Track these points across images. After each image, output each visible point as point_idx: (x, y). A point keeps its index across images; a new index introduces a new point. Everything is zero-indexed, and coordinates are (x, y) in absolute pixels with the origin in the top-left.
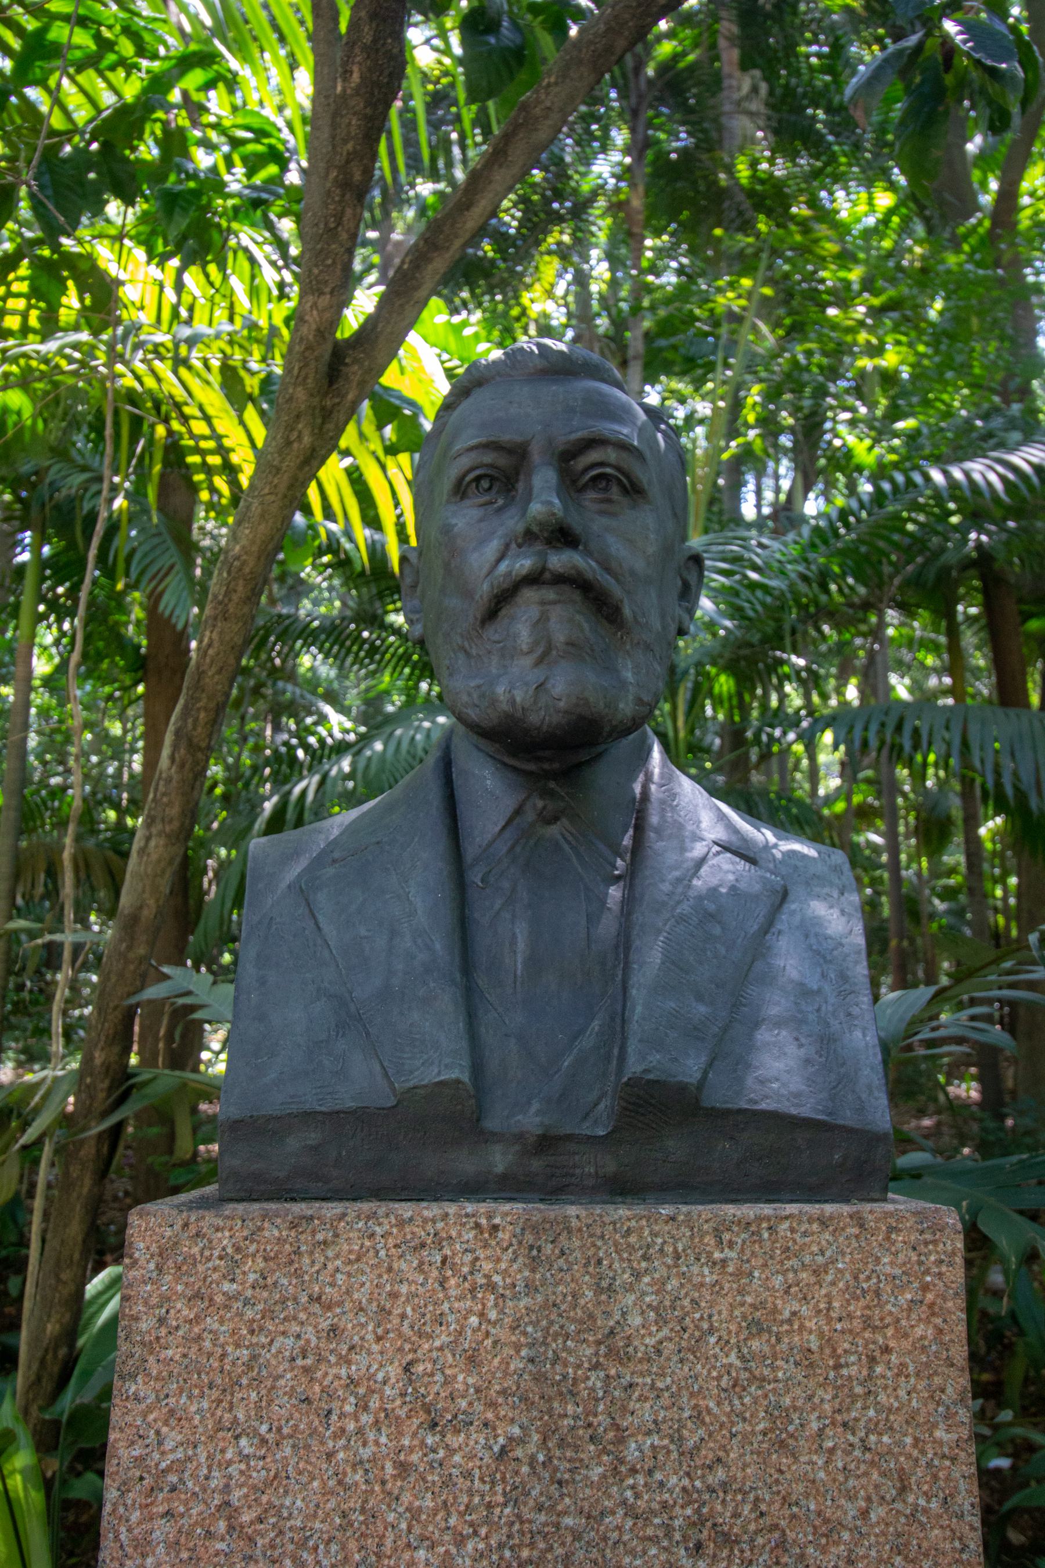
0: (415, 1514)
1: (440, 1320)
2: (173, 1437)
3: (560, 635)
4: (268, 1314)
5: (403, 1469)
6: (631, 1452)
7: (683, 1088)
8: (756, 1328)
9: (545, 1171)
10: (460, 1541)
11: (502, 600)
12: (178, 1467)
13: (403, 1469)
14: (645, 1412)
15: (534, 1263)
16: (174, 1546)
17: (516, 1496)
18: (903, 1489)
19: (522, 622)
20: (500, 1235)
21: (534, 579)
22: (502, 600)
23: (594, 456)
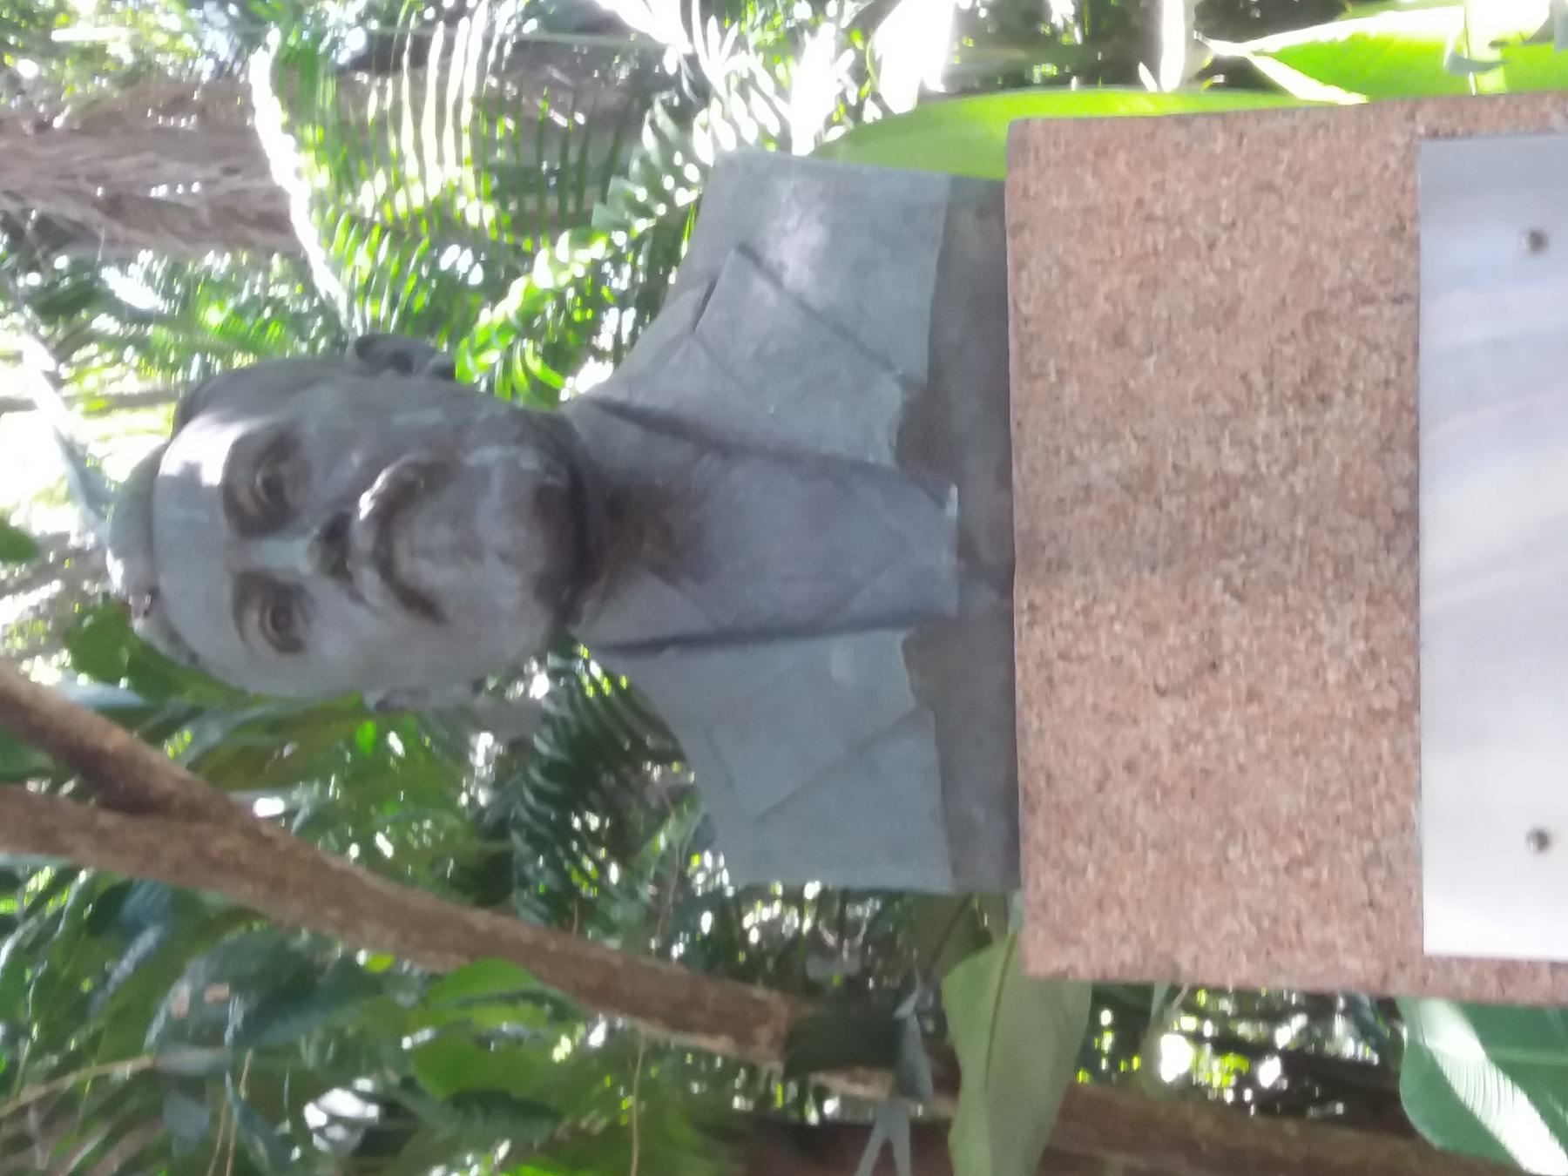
0: (1294, 684)
1: (1117, 661)
3: (442, 535)
4: (1114, 832)
5: (1253, 695)
6: (1236, 467)
8: (1119, 339)
9: (992, 565)
10: (1318, 639)
12: (1255, 918)
13: (1253, 695)
16: (1325, 920)
17: (1277, 584)
18: (1269, 187)
19: (433, 575)
21: (386, 568)
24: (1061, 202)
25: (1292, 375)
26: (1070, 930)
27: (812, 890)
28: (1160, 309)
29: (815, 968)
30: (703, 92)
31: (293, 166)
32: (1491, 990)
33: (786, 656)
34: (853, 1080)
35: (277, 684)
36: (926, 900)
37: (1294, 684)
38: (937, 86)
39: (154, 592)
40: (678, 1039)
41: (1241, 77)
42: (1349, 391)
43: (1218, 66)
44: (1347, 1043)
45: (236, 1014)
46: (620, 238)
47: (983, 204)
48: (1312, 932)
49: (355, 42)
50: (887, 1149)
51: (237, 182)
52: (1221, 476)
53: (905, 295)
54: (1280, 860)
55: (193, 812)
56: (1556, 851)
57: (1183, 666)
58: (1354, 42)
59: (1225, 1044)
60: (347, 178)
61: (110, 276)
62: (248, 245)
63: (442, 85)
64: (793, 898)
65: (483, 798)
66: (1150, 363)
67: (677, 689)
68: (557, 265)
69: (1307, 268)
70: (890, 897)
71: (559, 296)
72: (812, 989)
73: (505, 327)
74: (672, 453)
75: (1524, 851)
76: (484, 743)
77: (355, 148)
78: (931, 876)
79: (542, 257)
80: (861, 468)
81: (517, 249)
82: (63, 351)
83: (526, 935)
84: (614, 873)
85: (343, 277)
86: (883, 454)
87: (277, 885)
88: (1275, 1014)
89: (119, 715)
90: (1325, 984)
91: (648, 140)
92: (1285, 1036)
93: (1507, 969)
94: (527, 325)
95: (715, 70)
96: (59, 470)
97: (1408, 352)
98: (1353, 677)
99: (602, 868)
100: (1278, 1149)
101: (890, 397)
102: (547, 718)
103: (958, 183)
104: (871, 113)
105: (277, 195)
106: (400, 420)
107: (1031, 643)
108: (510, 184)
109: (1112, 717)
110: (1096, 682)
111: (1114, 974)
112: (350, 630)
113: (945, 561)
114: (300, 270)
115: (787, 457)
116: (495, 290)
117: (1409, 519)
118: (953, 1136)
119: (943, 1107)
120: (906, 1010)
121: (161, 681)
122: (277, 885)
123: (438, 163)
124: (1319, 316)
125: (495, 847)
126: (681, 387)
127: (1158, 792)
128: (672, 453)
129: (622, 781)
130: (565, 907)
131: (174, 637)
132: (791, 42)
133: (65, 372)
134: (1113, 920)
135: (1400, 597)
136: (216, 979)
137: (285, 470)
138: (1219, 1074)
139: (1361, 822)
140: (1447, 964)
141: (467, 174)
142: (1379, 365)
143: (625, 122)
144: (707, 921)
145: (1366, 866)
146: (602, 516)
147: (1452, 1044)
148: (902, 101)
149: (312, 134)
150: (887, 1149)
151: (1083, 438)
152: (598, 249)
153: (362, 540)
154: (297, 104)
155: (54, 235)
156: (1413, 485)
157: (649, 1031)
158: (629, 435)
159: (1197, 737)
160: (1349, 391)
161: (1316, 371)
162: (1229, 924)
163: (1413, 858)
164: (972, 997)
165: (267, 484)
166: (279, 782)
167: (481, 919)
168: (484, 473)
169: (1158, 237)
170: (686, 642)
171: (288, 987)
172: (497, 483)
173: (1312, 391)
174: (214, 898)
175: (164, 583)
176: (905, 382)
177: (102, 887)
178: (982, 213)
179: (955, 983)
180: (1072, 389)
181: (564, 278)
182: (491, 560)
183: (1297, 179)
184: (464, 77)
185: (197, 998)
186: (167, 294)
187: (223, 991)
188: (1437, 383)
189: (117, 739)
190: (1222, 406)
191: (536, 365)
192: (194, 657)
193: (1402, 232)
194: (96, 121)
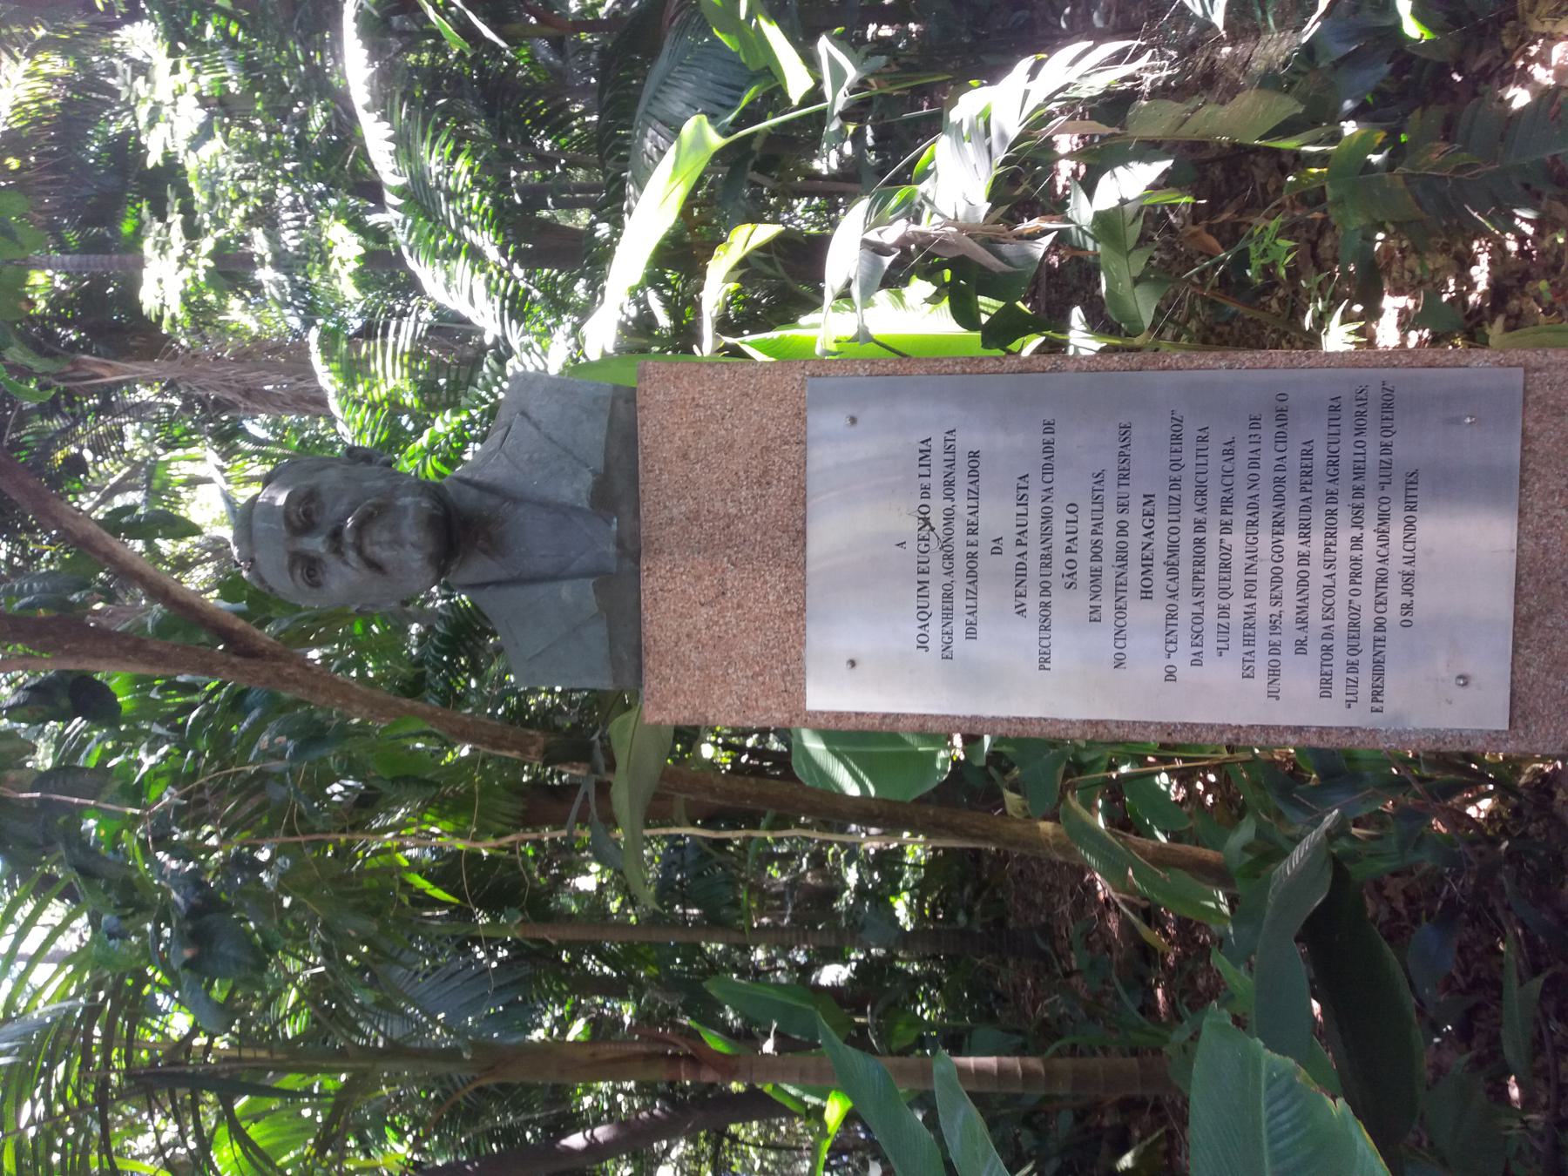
0: (756, 601)
1: (684, 591)
2: (728, 700)
3: (385, 536)
4: (682, 663)
5: (739, 606)
6: (733, 511)
7: (595, 483)
8: (685, 456)
9: (631, 550)
10: (766, 582)
11: (375, 566)
12: (739, 698)
13: (739, 606)
14: (718, 505)
15: (661, 551)
16: (767, 698)
17: (749, 560)
18: (747, 395)
19: (382, 554)
20: (1525, 812)
21: (360, 551)
22: (375, 566)
23: (294, 517)
24: (660, 397)
25: (757, 473)
26: (664, 703)
27: (558, 689)
28: (702, 445)
29: (558, 720)
30: (510, 352)
31: (327, 378)
32: (832, 725)
33: (541, 590)
34: (572, 767)
35: (312, 602)
36: (605, 692)
37: (756, 601)
38: (610, 350)
39: (252, 560)
40: (497, 752)
41: (736, 352)
42: (779, 480)
43: (727, 347)
44: (775, 746)
45: (291, 745)
46: (474, 412)
47: (627, 398)
48: (762, 703)
49: (358, 324)
50: (586, 794)
51: (303, 384)
52: (727, 515)
53: (593, 435)
54: (750, 673)
55: (275, 657)
56: (858, 667)
57: (712, 593)
58: (781, 339)
59: (726, 746)
60: (351, 383)
61: (247, 424)
62: (307, 412)
63: (395, 345)
64: (551, 691)
65: (414, 651)
66: (698, 466)
67: (496, 604)
68: (444, 423)
69: (762, 429)
70: (592, 691)
71: (447, 436)
72: (557, 729)
73: (422, 449)
74: (491, 501)
75: (844, 666)
76: (415, 628)
77: (354, 370)
78: (605, 683)
79: (438, 420)
80: (574, 509)
81: (428, 417)
82: (225, 456)
83: (427, 709)
84: (473, 684)
85: (350, 427)
86: (584, 504)
87: (313, 688)
88: (747, 734)
89: (239, 614)
90: (766, 724)
91: (485, 369)
92: (750, 742)
93: (839, 716)
94: (430, 450)
95: (515, 341)
96: (221, 506)
97: (802, 465)
98: (780, 597)
99: (468, 682)
100: (747, 789)
101: (588, 478)
102: (441, 617)
103: (616, 388)
104: (583, 360)
105: (320, 390)
106: (366, 484)
107: (648, 584)
108: (426, 388)
109: (681, 615)
110: (674, 600)
111: (681, 723)
112: (343, 577)
113: (612, 549)
114: (332, 421)
115: (543, 504)
116: (419, 432)
117: (802, 533)
118: (613, 789)
119: (608, 778)
120: (595, 737)
121: (261, 603)
122: (313, 688)
123: (392, 378)
124: (767, 448)
125: (418, 670)
126: (497, 473)
127: (700, 646)
128: (491, 501)
129: (476, 644)
130: (451, 699)
131: (262, 581)
132: (548, 333)
133: (226, 466)
134: (681, 700)
135: (798, 565)
136: (280, 734)
137: (313, 506)
138: (725, 759)
139: (782, 657)
140: (815, 714)
141: (405, 384)
142: (791, 470)
143: (476, 363)
144: (514, 701)
145: (783, 675)
146: (460, 525)
147: (815, 746)
148: (594, 355)
149: (335, 366)
150: (586, 794)
151: (670, 498)
152: (464, 417)
153: (349, 538)
154: (328, 350)
155: (221, 405)
156: (804, 519)
157: (484, 750)
158: (472, 493)
159: (716, 623)
160: (779, 480)
161: (765, 472)
162: (728, 700)
163: (802, 672)
164: (621, 731)
165: (304, 513)
166: (318, 644)
167: (407, 702)
168: (405, 508)
169: (700, 414)
170: (498, 583)
171: (313, 736)
172: (411, 512)
173: (764, 480)
174: (287, 695)
175: (257, 556)
176: (594, 472)
177: (237, 690)
178: (627, 401)
179: (614, 727)
180: (665, 476)
181: (449, 428)
182: (408, 547)
183: (758, 391)
184: (405, 342)
185: (271, 740)
186: (274, 433)
187: (284, 739)
188: (813, 485)
189: (240, 624)
190: (728, 486)
191: (438, 466)
192: (271, 590)
193: (800, 415)
194: (242, 356)
